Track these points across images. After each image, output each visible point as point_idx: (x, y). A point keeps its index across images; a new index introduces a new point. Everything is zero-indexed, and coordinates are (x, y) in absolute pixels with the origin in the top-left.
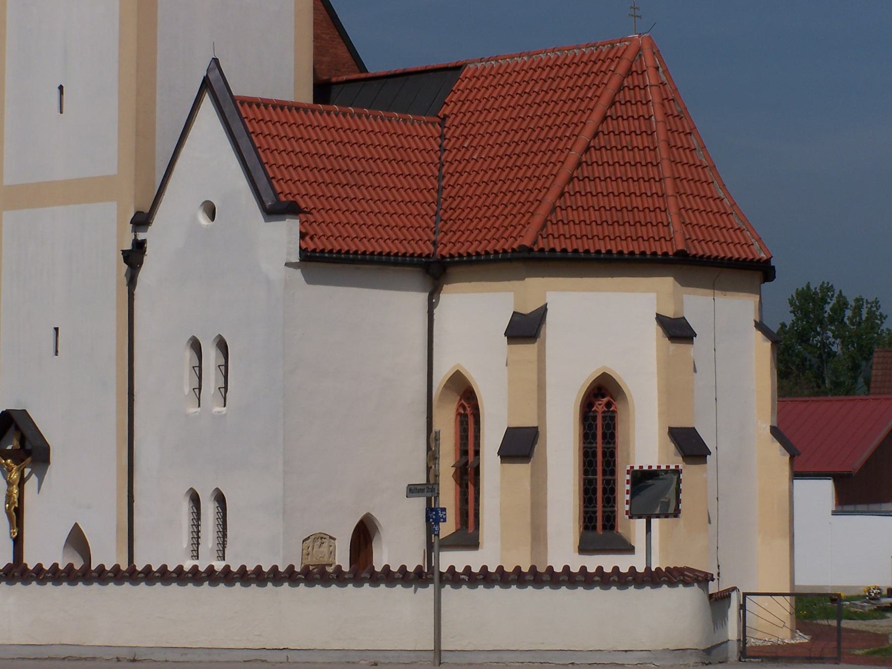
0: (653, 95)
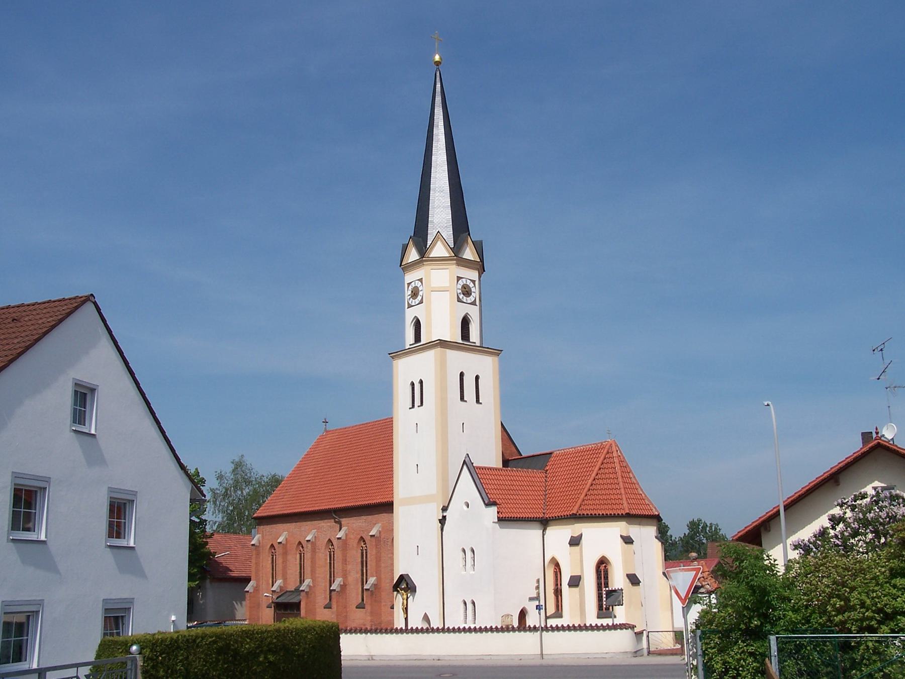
0: (616, 460)
